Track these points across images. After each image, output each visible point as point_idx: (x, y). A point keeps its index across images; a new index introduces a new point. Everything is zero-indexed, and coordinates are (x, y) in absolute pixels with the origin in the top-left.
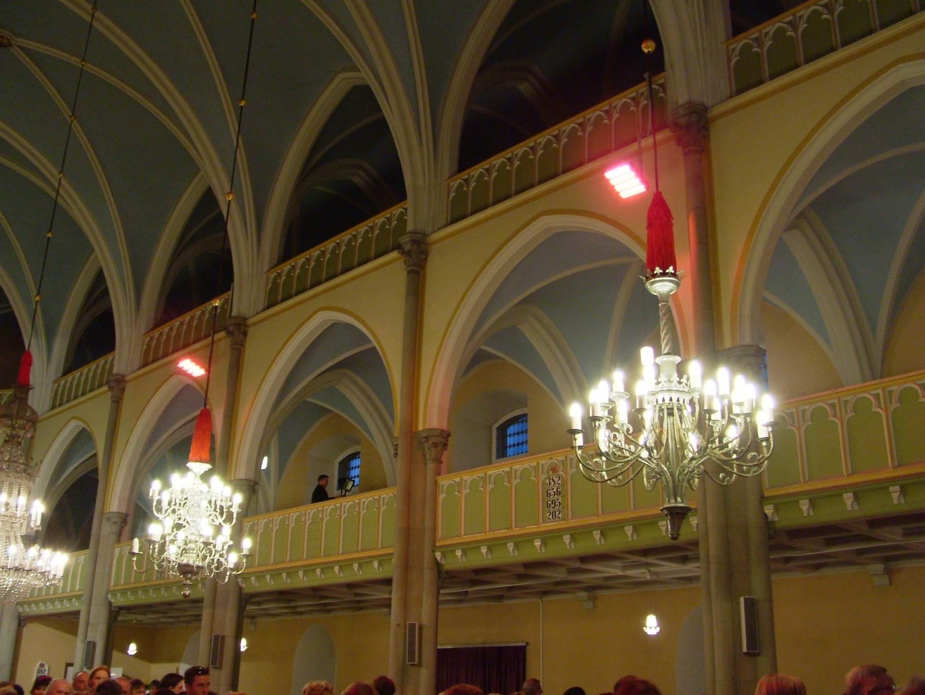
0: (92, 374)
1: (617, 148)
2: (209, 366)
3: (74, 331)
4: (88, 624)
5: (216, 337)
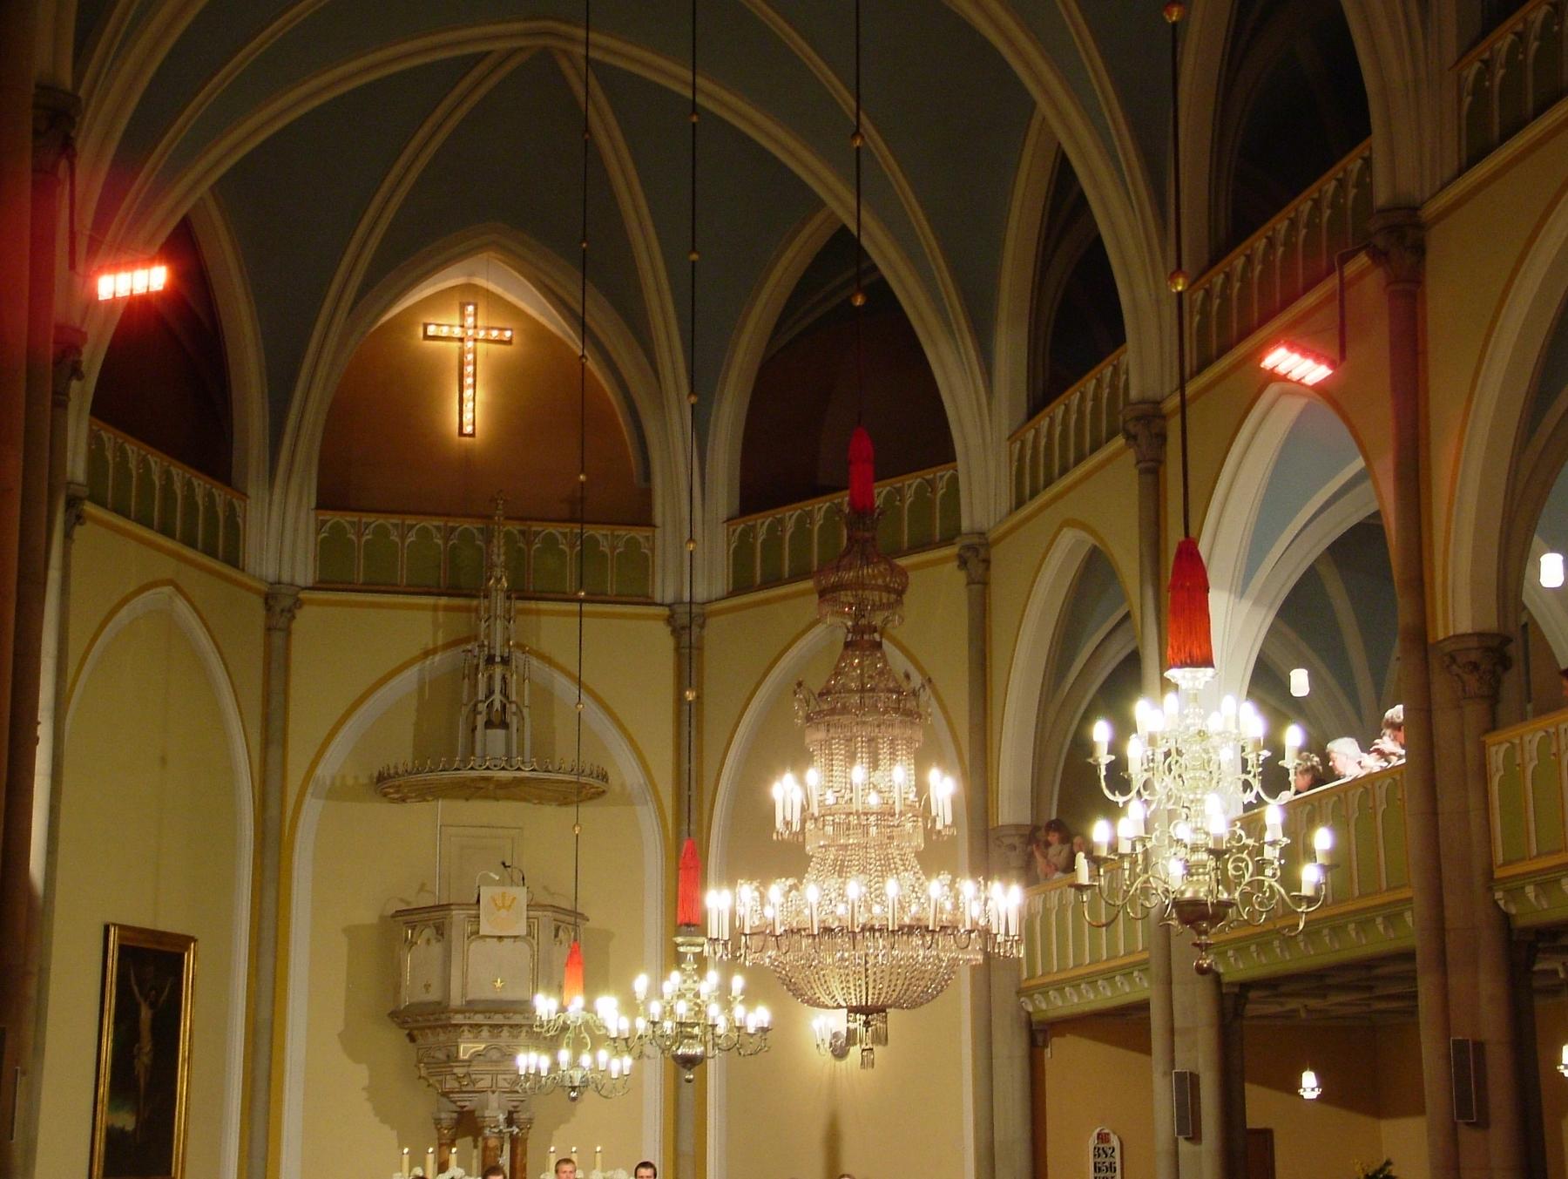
0: (1089, 404)
1: (1265, 319)
2: (1338, 355)
3: (1039, 286)
4: (1171, 1031)
5: (1351, 269)
